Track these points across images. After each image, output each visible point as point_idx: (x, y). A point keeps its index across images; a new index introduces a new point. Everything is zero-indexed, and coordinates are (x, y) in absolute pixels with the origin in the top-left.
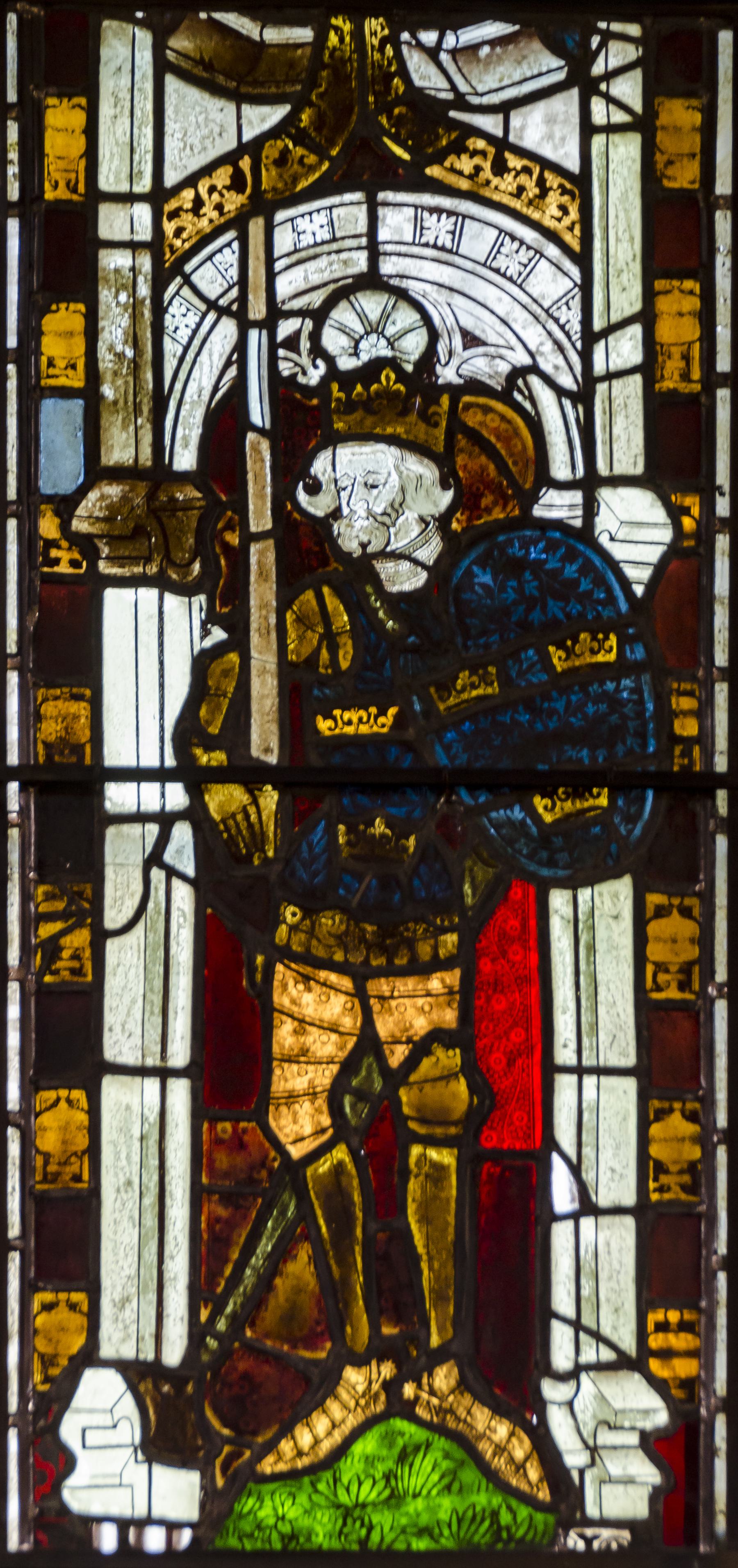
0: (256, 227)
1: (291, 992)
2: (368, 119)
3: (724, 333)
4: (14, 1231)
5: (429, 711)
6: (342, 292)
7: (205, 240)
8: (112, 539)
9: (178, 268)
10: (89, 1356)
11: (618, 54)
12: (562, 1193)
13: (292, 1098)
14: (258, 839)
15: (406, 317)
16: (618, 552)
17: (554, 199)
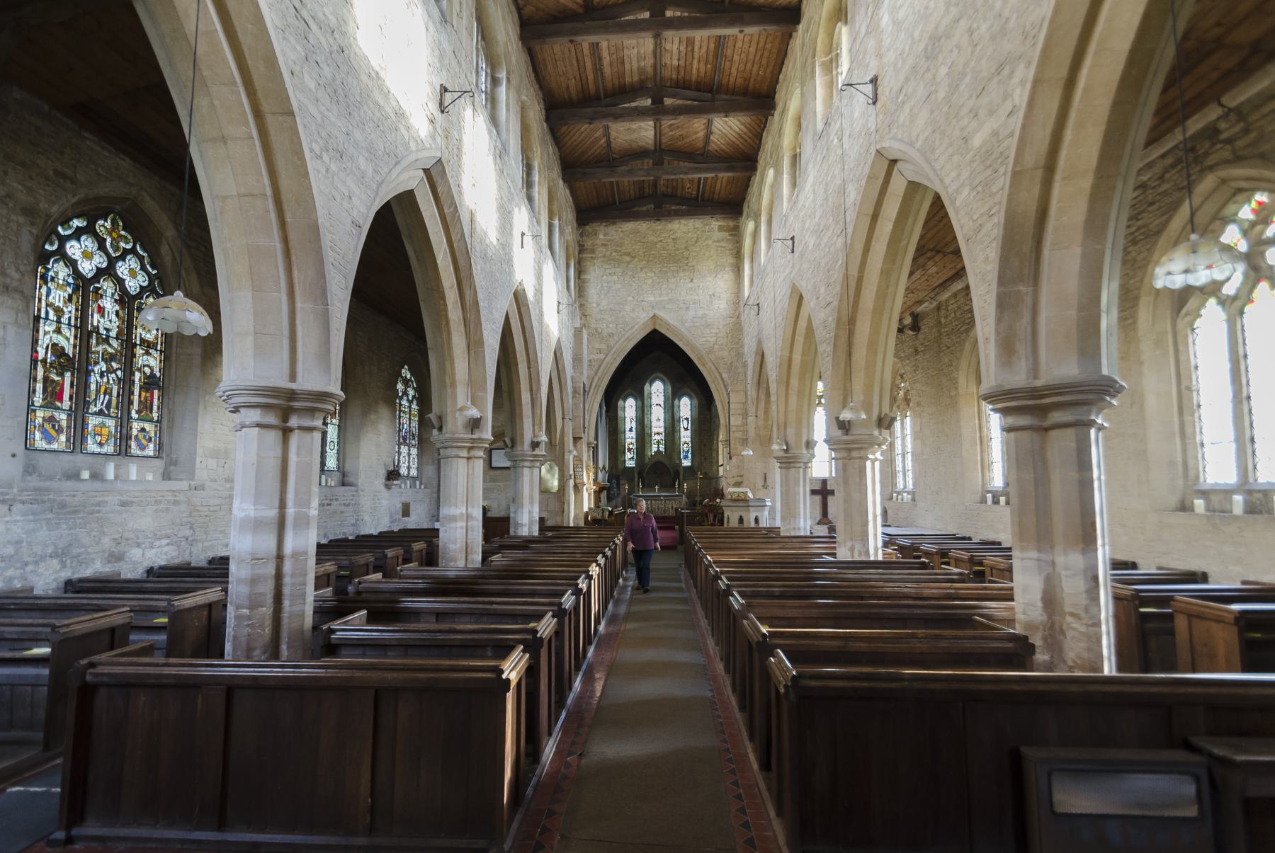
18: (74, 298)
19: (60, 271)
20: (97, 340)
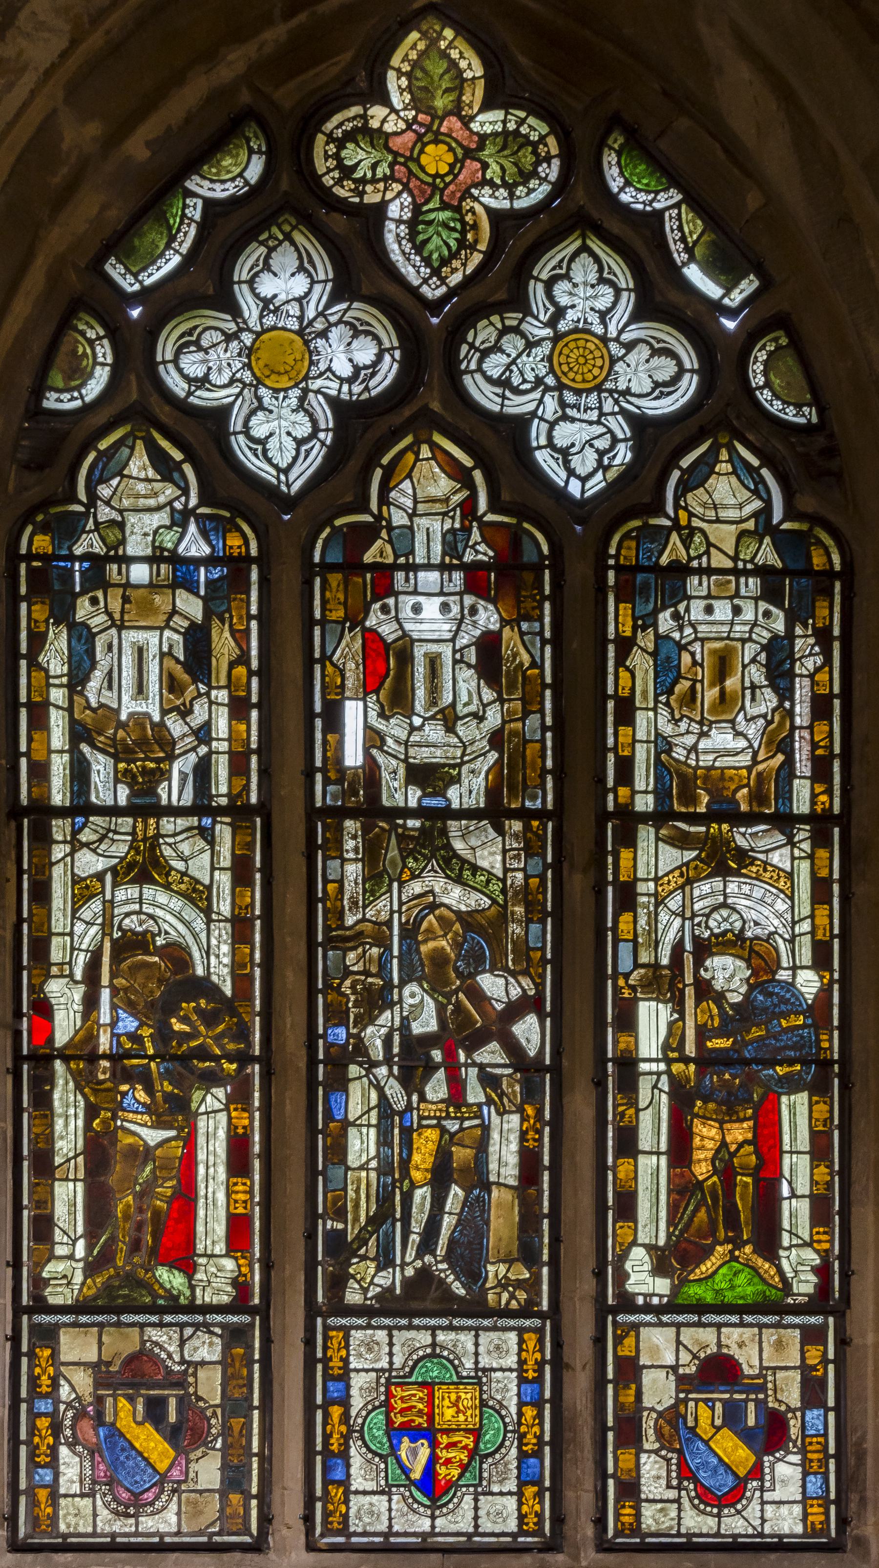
0: (687, 889)
1: (698, 1127)
2: (723, 855)
3: (836, 921)
4: (610, 1203)
5: (743, 1039)
6: (715, 909)
7: (671, 893)
8: (642, 986)
9: (662, 902)
10: (634, 1243)
11: (802, 835)
12: (785, 1191)
13: (699, 1161)
14: (688, 1080)
15: (735, 916)
16: (803, 990)
17: (782, 880)
18: (223, 644)
19: (142, 508)
20: (371, 854)
